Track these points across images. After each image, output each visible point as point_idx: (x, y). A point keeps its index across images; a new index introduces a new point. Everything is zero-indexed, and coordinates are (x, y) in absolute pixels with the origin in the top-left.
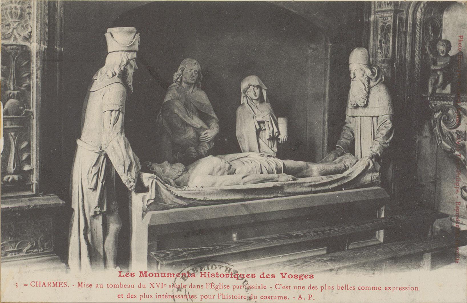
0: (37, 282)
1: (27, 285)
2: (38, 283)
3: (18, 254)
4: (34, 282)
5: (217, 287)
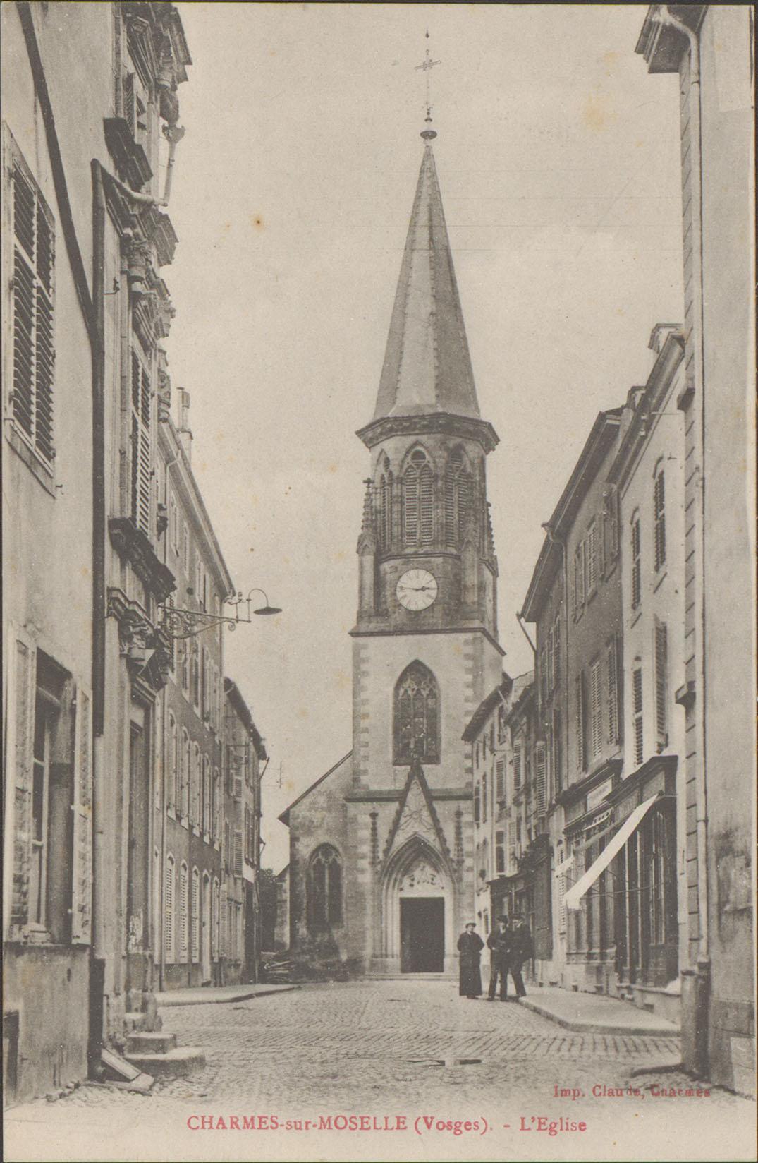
0: (203, 1117)
1: (562, 975)
2: (207, 1119)
3: (653, 397)
4: (197, 1118)
5: (553, 1125)
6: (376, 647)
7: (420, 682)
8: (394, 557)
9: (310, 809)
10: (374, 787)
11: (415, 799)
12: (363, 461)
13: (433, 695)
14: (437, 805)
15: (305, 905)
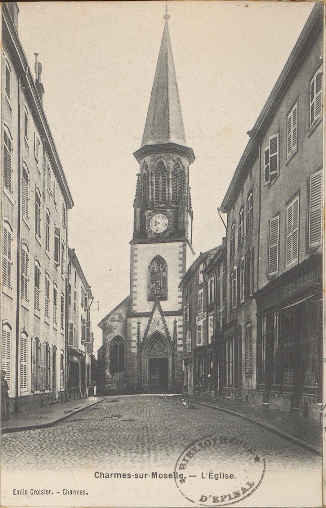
6: (141, 247)
7: (160, 265)
8: (150, 209)
9: (111, 321)
10: (139, 311)
11: (157, 315)
12: (135, 167)
13: (165, 270)
14: (166, 318)
15: (109, 362)
